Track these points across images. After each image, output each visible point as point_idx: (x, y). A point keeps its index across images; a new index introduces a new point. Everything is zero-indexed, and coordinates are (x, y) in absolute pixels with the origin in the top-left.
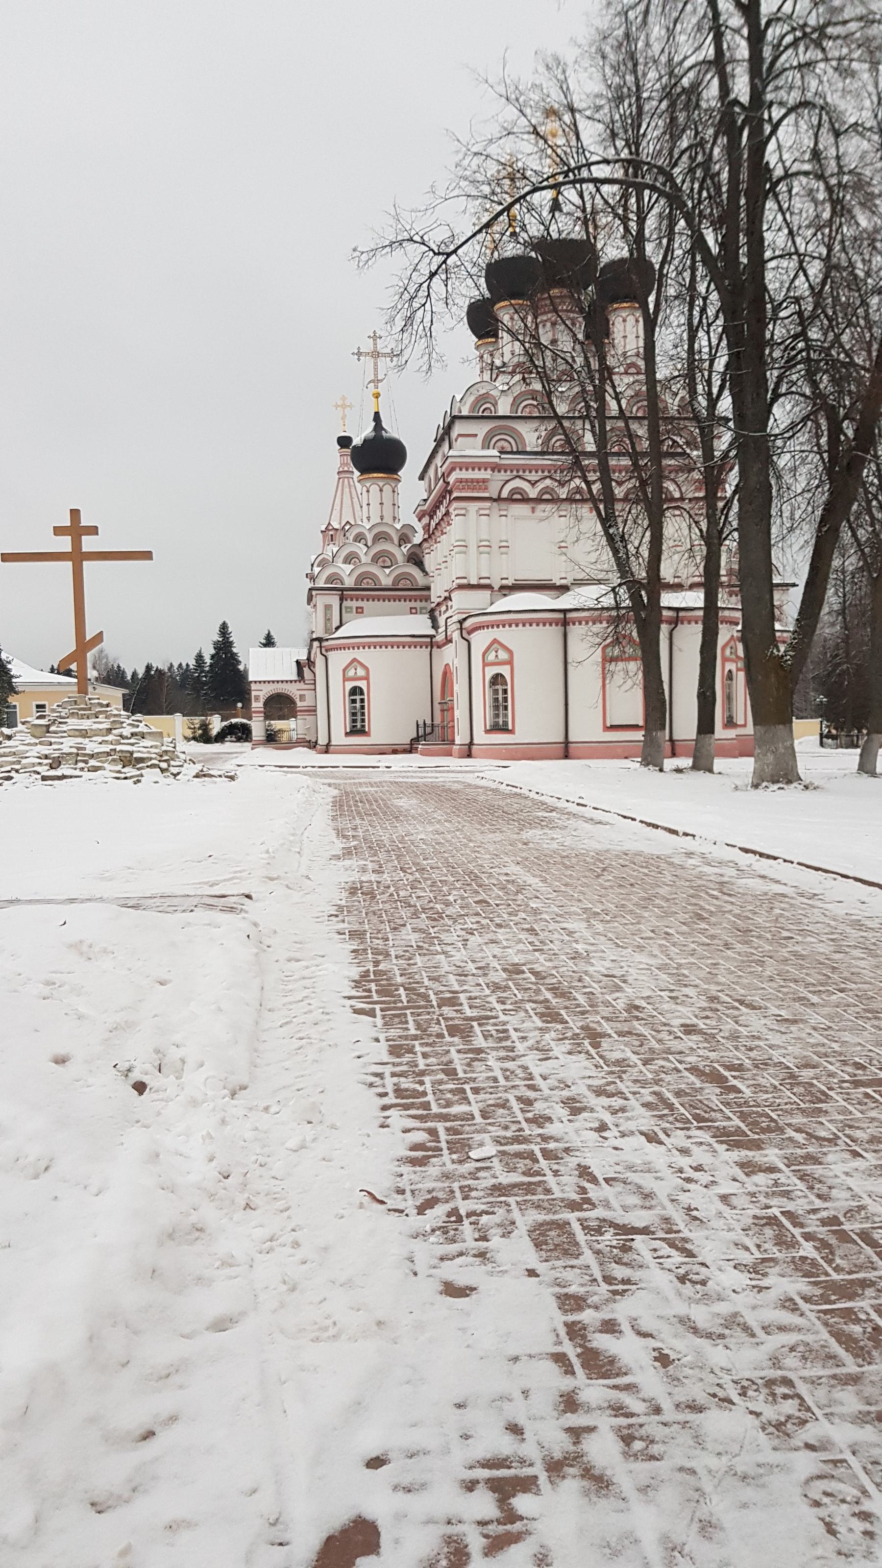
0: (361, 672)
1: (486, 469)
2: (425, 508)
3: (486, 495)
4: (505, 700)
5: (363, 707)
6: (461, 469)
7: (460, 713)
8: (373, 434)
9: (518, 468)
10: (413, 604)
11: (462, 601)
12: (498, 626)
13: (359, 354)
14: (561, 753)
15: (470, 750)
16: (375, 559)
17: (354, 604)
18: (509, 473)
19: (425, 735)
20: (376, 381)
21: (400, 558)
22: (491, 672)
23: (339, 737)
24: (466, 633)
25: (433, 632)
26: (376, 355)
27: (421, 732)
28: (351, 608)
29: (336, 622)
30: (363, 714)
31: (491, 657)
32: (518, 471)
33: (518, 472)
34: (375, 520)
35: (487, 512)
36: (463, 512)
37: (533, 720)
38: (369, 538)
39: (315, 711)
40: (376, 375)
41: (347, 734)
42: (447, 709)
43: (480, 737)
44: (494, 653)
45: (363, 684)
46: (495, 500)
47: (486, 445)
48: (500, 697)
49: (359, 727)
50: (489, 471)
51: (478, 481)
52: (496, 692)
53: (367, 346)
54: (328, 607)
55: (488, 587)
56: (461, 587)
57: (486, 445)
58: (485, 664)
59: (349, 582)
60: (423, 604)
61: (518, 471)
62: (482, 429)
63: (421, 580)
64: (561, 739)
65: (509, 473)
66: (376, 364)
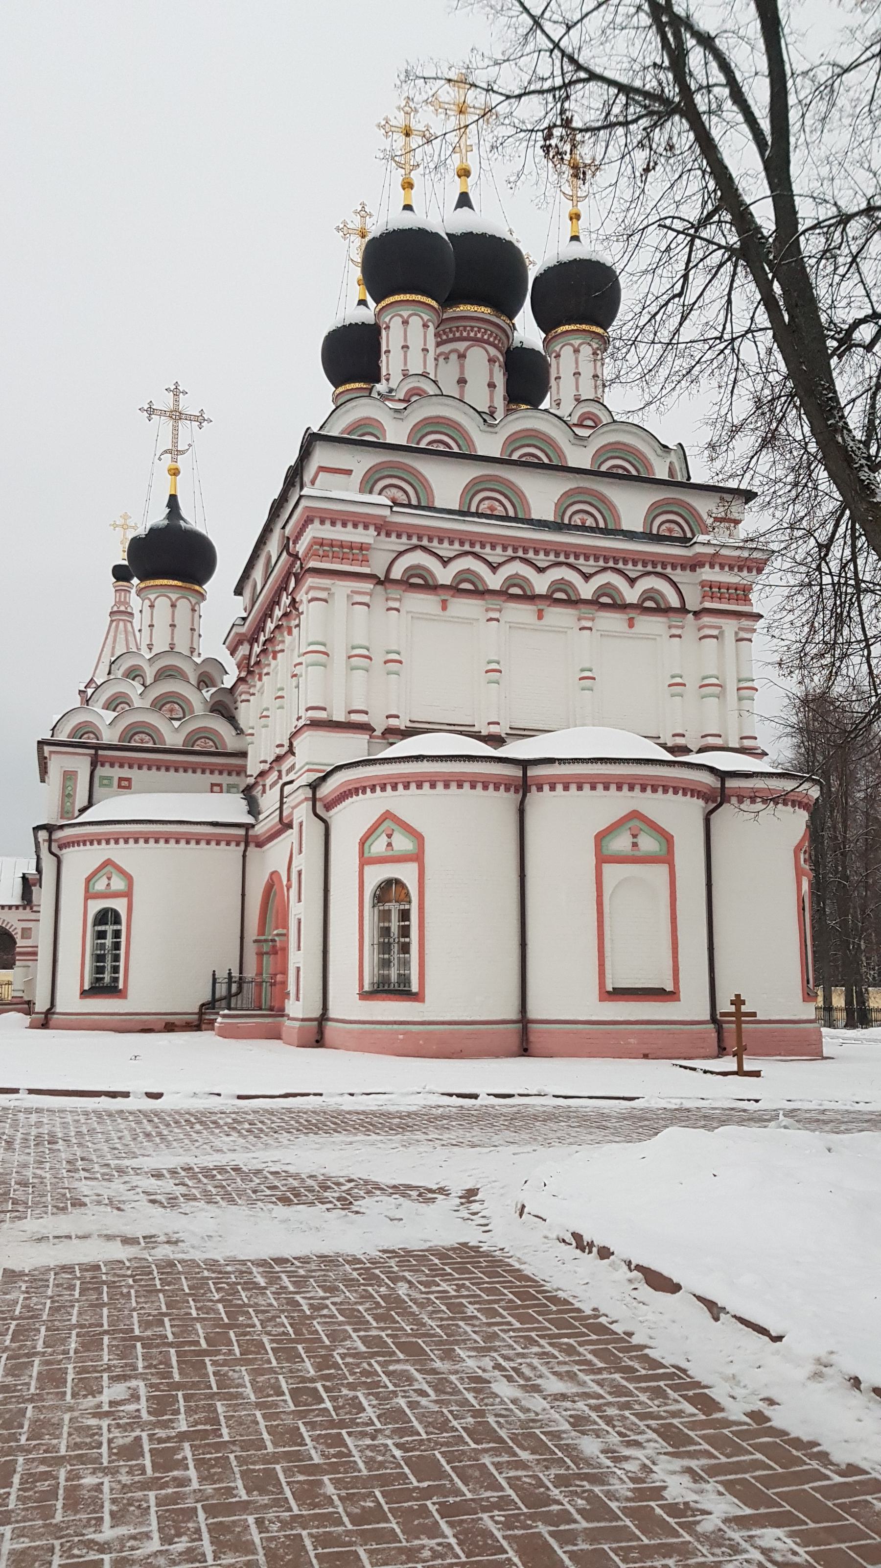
0: (118, 884)
1: (366, 527)
2: (243, 630)
3: (367, 570)
4: (405, 931)
5: (117, 946)
6: (322, 522)
7: (301, 959)
8: (166, 522)
9: (420, 533)
10: (216, 778)
11: (318, 750)
12: (395, 787)
13: (151, 411)
14: (513, 1042)
15: (321, 1031)
16: (158, 705)
17: (117, 773)
18: (404, 539)
19: (229, 996)
20: (175, 452)
21: (198, 707)
22: (376, 875)
23: (69, 999)
24: (322, 807)
25: (250, 820)
26: (176, 415)
27: (222, 990)
28: (110, 778)
29: (81, 799)
30: (116, 958)
31: (378, 847)
32: (420, 538)
33: (420, 538)
34: (161, 646)
35: (366, 599)
36: (323, 595)
37: (460, 977)
38: (150, 674)
39: (35, 954)
40: (175, 443)
41: (84, 994)
42: (275, 950)
43: (346, 1004)
44: (384, 839)
45: (119, 905)
46: (380, 582)
47: (368, 484)
48: (394, 925)
49: (394, 977)
50: (372, 531)
51: (351, 546)
52: (385, 916)
53: (165, 402)
54: (69, 776)
55: (365, 728)
56: (315, 724)
57: (368, 484)
58: (365, 861)
59: (109, 736)
60: (234, 779)
61: (420, 538)
62: (361, 463)
63: (231, 742)
64: (512, 1013)
65: (404, 539)
66: (175, 429)
